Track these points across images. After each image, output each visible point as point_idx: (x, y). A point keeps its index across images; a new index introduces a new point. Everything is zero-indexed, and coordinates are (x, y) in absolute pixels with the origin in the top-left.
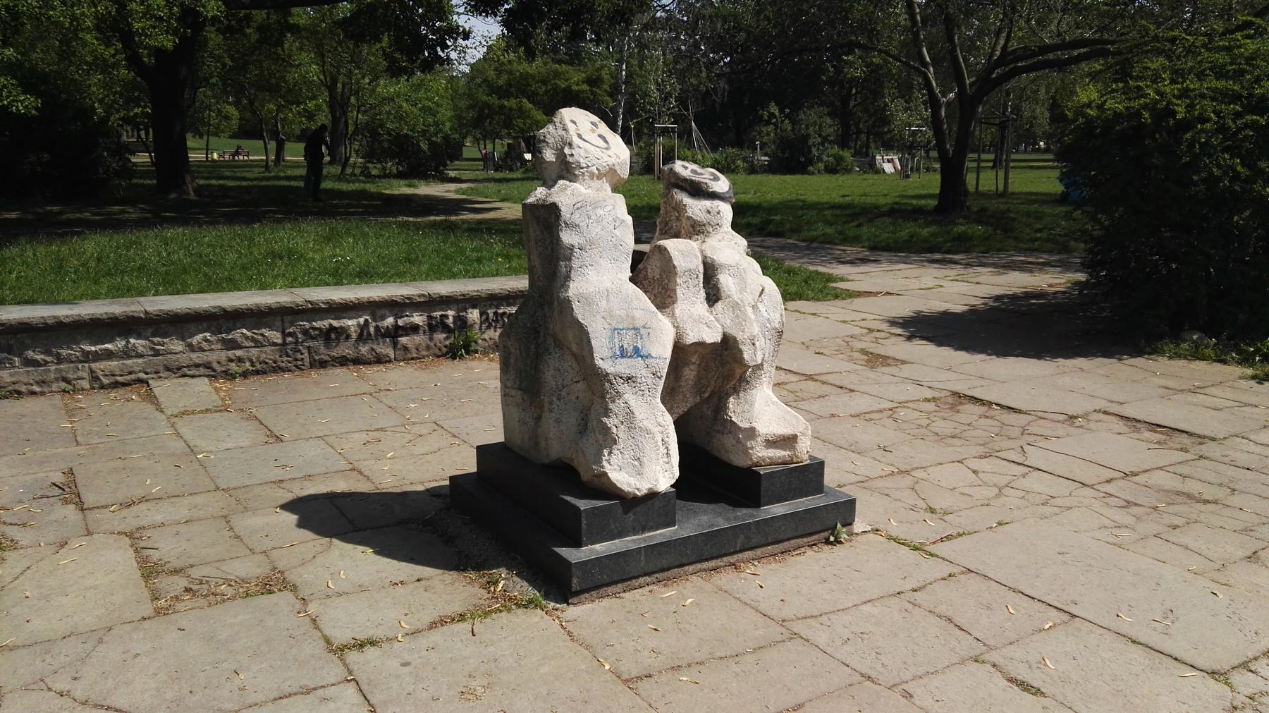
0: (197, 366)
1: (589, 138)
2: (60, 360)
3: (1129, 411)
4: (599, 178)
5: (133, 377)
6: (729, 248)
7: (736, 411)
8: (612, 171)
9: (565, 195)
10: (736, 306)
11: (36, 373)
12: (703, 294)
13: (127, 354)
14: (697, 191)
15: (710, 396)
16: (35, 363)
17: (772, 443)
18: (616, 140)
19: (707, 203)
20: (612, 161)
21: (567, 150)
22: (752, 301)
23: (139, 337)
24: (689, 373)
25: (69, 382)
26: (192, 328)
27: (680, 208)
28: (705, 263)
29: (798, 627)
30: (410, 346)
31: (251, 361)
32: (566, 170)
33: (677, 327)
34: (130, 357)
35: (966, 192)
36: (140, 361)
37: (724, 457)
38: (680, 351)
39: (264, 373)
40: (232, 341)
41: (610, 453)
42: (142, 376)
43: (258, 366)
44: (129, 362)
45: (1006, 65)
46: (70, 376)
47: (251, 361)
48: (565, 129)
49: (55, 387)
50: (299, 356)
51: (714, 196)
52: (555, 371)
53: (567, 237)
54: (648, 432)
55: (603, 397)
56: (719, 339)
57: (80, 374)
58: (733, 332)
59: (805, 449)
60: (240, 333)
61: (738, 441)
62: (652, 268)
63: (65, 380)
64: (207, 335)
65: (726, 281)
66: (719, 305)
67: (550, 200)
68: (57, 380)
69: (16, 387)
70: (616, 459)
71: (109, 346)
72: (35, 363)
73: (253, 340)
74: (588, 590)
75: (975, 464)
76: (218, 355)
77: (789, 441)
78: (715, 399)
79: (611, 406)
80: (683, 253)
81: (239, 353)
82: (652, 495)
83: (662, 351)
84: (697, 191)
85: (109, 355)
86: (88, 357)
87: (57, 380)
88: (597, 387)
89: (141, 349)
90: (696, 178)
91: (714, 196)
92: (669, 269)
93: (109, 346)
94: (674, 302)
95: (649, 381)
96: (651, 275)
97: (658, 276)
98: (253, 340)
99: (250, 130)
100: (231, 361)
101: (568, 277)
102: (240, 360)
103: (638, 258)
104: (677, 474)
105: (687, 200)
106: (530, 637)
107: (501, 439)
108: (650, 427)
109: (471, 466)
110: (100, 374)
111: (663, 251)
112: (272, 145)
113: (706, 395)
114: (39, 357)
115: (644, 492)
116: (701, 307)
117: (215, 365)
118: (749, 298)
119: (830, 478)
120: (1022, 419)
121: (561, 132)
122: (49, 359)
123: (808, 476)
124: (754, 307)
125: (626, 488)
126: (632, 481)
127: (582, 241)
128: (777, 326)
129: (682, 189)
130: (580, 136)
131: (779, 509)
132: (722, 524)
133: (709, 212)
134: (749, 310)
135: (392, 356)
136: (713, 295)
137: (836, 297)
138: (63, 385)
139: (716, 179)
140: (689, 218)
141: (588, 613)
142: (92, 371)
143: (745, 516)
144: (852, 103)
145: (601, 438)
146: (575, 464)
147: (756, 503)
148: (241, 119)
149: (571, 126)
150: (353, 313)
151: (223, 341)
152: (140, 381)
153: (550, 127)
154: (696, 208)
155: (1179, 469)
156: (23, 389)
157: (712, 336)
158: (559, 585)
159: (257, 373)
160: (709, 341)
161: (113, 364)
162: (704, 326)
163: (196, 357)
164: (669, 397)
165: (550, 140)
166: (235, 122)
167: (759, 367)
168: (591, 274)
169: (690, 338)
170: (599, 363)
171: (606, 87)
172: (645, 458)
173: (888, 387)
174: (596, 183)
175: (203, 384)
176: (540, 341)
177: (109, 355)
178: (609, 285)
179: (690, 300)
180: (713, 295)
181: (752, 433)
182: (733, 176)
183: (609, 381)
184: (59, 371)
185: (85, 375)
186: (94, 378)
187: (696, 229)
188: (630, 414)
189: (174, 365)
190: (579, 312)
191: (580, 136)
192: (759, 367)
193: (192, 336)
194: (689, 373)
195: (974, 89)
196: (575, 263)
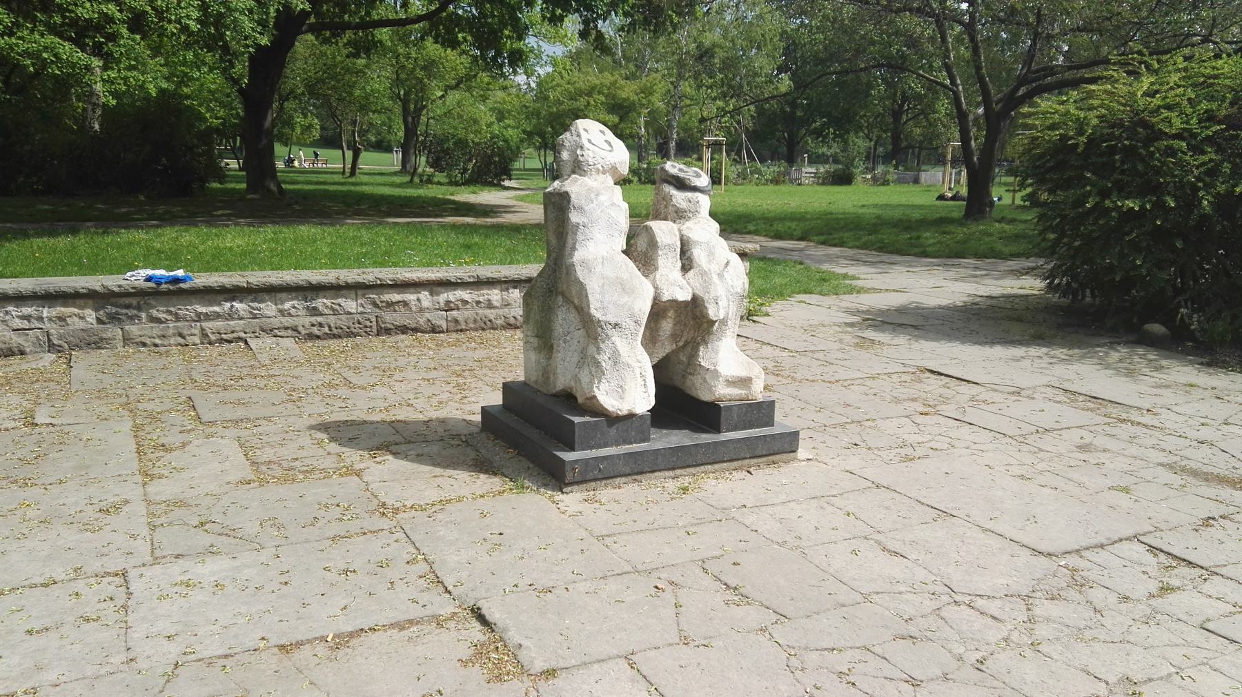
0: (286, 328)
1: (598, 143)
2: (178, 318)
3: (1067, 386)
4: (604, 173)
5: (235, 335)
6: (704, 230)
7: (705, 358)
8: (613, 170)
9: (574, 186)
10: (704, 274)
11: (157, 329)
12: (679, 264)
13: (230, 316)
14: (681, 184)
15: (685, 345)
16: (159, 321)
17: (731, 383)
18: (619, 144)
19: (690, 195)
20: (616, 160)
21: (579, 152)
22: (723, 273)
23: (241, 302)
24: (667, 326)
25: (184, 337)
26: (284, 295)
27: (667, 199)
28: (681, 240)
29: (734, 513)
30: (460, 319)
31: (330, 327)
32: (578, 167)
33: (656, 288)
34: (233, 319)
35: (992, 203)
36: (241, 322)
37: (694, 393)
38: (659, 310)
39: (340, 337)
40: (315, 309)
41: (600, 381)
42: (243, 335)
43: (335, 331)
44: (232, 323)
45: (1030, 82)
46: (185, 332)
47: (330, 327)
48: (579, 135)
49: (172, 341)
50: (368, 323)
51: (695, 189)
52: (563, 319)
53: (574, 217)
54: (629, 366)
55: (596, 339)
56: (689, 298)
57: (194, 331)
58: (700, 293)
59: (758, 392)
60: (322, 303)
61: (705, 381)
62: (641, 243)
64: (295, 302)
65: (698, 253)
66: (691, 273)
67: (564, 189)
68: (174, 335)
69: (143, 339)
70: (604, 386)
71: (217, 309)
72: (159, 321)
73: (332, 309)
74: (578, 483)
75: (920, 419)
76: (304, 321)
77: (745, 382)
78: (689, 349)
79: (602, 345)
80: (665, 231)
81: (320, 319)
82: (631, 416)
83: (644, 307)
84: (681, 184)
85: (217, 316)
86: (199, 317)
87: (174, 335)
88: (591, 329)
89: (242, 313)
90: (681, 175)
91: (695, 189)
92: (653, 244)
93: (217, 309)
94: (656, 269)
96: (640, 250)
97: (646, 249)
98: (332, 309)
99: (330, 141)
100: (313, 325)
101: (574, 248)
102: (321, 325)
103: (630, 237)
104: (653, 403)
105: (674, 192)
106: (530, 509)
107: (522, 379)
108: (630, 362)
109: (496, 399)
110: (209, 332)
111: (648, 229)
112: (349, 154)
113: (681, 344)
114: (162, 316)
115: (625, 412)
116: (676, 273)
117: (300, 329)
118: (714, 268)
119: (778, 417)
120: (975, 390)
121: (575, 138)
122: (169, 317)
123: (761, 412)
124: (720, 276)
125: (610, 409)
127: (586, 221)
129: (670, 183)
130: (589, 141)
132: (687, 442)
134: (715, 278)
135: (445, 327)
136: (687, 264)
137: (859, 292)
139: (698, 176)
140: (674, 206)
141: (572, 499)
142: (202, 329)
144: (904, 118)
145: (593, 369)
146: (574, 391)
147: (718, 430)
148: (322, 128)
149: (583, 133)
150: (412, 290)
151: (307, 308)
152: (240, 339)
153: (568, 134)
154: (679, 198)
155: (1092, 429)
156: (148, 341)
157: (684, 296)
158: (556, 477)
159: (335, 336)
160: (681, 299)
161: (219, 324)
162: (678, 289)
163: (287, 321)
164: (650, 340)
165: (567, 144)
166: (316, 134)
167: (724, 322)
168: (591, 245)
169: (666, 297)
170: (593, 311)
171: (1214, 106)
172: (629, 388)
173: (868, 362)
174: (601, 177)
175: (289, 343)
176: (553, 296)
177: (217, 316)
178: (605, 254)
179: (668, 265)
180: (687, 264)
181: (716, 373)
184: (177, 327)
185: (197, 332)
186: (204, 335)
187: (680, 215)
188: (616, 352)
189: (267, 327)
190: (581, 273)
191: (589, 141)
192: (724, 322)
193: (282, 303)
194: (667, 326)
195: (999, 106)
196: (580, 237)
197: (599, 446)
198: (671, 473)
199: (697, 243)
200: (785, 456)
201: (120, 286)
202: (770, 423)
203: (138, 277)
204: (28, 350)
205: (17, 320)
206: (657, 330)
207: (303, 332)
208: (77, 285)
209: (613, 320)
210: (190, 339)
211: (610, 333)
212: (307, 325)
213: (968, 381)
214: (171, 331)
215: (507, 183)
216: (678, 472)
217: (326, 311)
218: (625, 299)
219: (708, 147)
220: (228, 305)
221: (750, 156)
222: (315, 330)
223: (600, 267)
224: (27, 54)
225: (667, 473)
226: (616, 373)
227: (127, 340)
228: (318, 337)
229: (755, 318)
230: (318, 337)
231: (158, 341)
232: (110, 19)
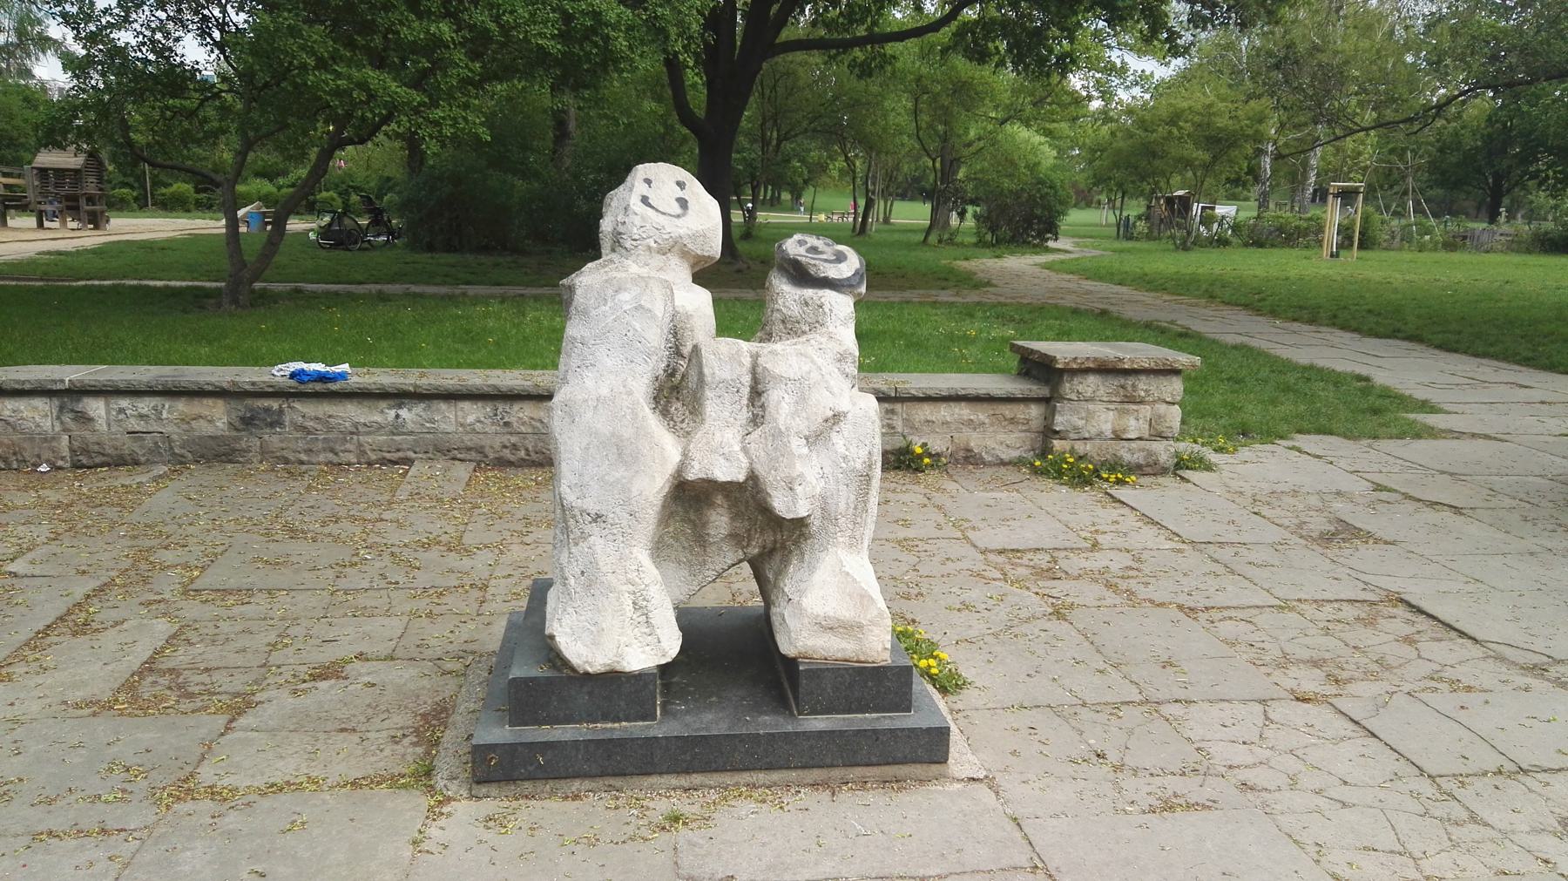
0: (469, 449)
5: (400, 454)
10: (778, 434)
19: (809, 293)
28: (754, 372)
33: (685, 455)
43: (534, 457)
46: (338, 447)
49: (321, 458)
57: (348, 446)
63: (332, 450)
69: (285, 453)
83: (653, 487)
91: (827, 283)
95: (625, 523)
96: (677, 391)
100: (505, 447)
110: (367, 448)
117: (487, 450)
122: (319, 427)
126: (584, 651)
128: (859, 466)
131: (819, 723)
132: (721, 728)
133: (807, 304)
137: (1418, 436)
138: (331, 456)
142: (360, 445)
143: (768, 723)
148: (340, 194)
156: (291, 457)
169: (692, 475)
182: (40, 115)
183: (574, 517)
197: (554, 721)
198: (684, 781)
199: (780, 379)
200: (918, 770)
201: (253, 384)
202: (903, 703)
203: (281, 373)
204: (143, 459)
205: (132, 420)
206: (705, 525)
207: (492, 456)
208: (201, 379)
209: (593, 507)
210: (345, 457)
211: (588, 529)
212: (497, 446)
213: (1462, 634)
214: (320, 445)
215: (1051, 244)
216: (697, 779)
217: (523, 429)
218: (620, 473)
219: (1336, 196)
220: (392, 413)
221: (1418, 210)
222: (507, 454)
223: (589, 414)
224: (337, 93)
225: (673, 780)
226: (589, 600)
227: (265, 452)
228: (510, 464)
229: (1187, 474)
230: (510, 464)
231: (304, 457)
232: (437, 42)
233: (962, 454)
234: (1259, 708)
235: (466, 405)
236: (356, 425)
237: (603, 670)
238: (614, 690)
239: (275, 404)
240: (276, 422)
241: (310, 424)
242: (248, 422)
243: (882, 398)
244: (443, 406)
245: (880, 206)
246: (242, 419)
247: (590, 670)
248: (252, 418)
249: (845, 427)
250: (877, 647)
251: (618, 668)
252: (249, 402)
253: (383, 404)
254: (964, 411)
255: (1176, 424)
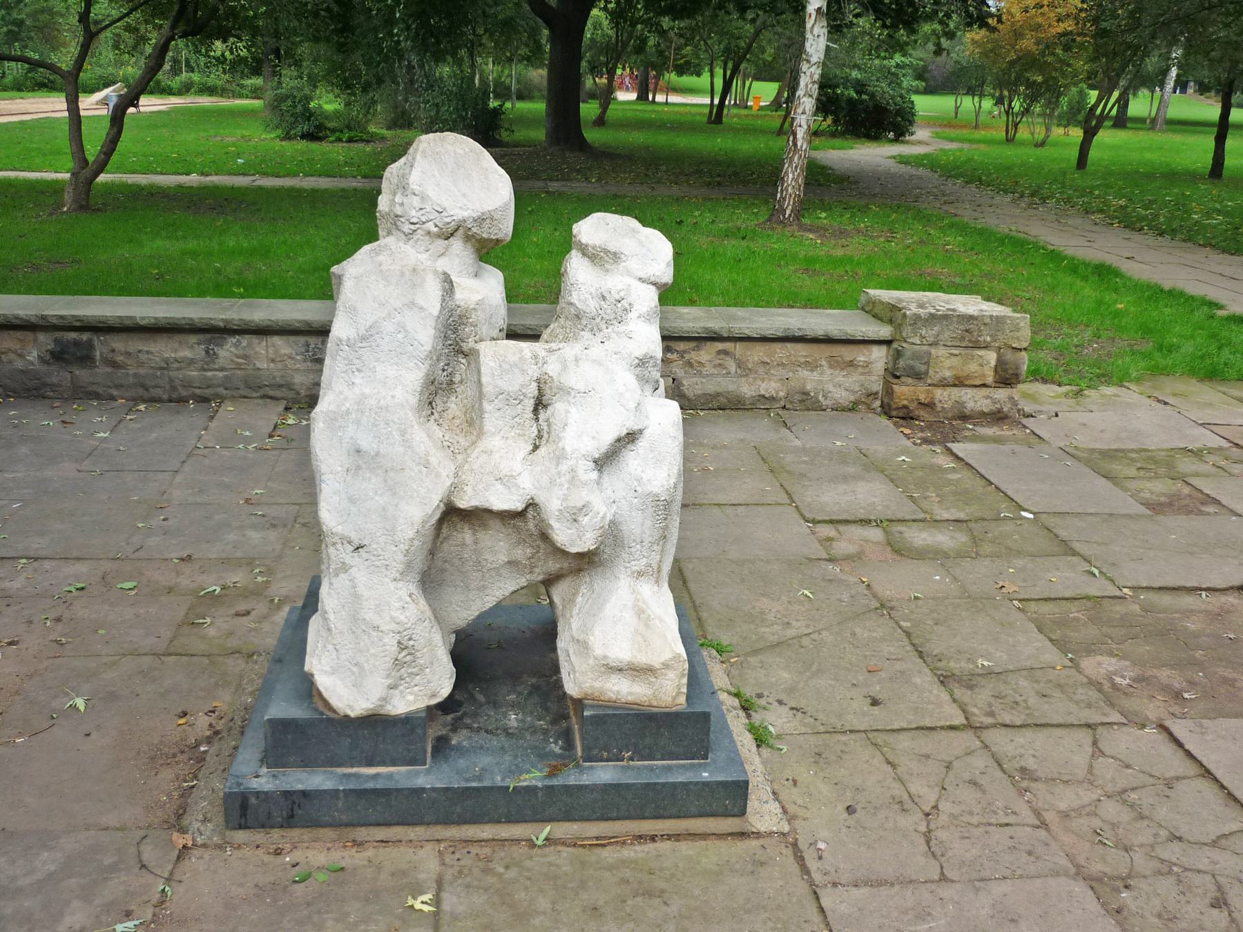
0: (281, 386)
83: (418, 510)
110: (177, 382)
133: (604, 298)
142: (171, 380)
201: (62, 317)
233: (798, 397)
234: (1085, 736)
235: (277, 340)
236: (166, 361)
237: (365, 713)
238: (376, 733)
239: (85, 337)
240: (86, 359)
241: (120, 358)
242: (59, 356)
243: (687, 404)
244: (255, 340)
245: (736, 84)
246: (52, 353)
247: (352, 715)
248: (62, 352)
249: (642, 444)
250: (669, 691)
251: (382, 712)
252: (58, 335)
253: (193, 339)
254: (801, 350)
255: (1026, 333)
